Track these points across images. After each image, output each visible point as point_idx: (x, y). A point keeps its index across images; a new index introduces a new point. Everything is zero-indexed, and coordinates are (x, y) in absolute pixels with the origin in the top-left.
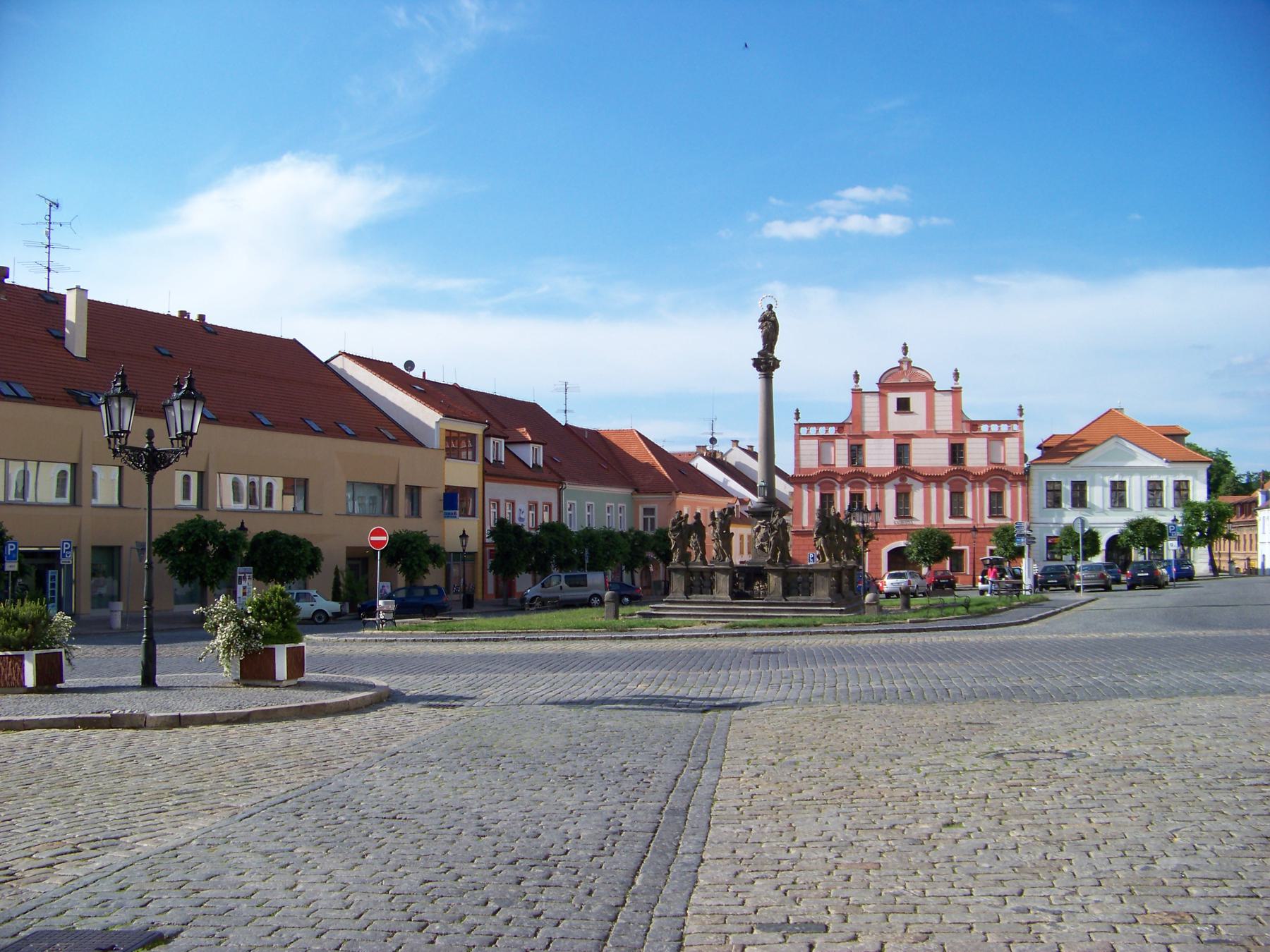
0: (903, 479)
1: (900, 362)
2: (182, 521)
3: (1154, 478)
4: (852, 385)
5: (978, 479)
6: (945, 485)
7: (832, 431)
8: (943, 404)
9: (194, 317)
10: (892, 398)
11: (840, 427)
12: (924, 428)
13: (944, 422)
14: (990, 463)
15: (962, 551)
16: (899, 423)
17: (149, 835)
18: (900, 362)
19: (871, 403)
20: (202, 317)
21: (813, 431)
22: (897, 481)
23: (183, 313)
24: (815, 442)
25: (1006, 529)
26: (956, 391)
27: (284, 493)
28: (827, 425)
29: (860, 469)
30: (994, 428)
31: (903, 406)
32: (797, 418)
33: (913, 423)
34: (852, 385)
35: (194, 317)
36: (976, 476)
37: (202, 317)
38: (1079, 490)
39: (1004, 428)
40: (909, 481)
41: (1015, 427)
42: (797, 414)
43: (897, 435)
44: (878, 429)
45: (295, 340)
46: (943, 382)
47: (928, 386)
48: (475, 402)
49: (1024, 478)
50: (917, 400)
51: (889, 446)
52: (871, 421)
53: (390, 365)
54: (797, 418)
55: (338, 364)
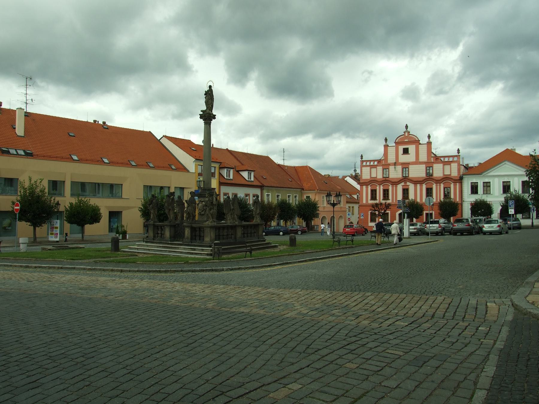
0: (405, 183)
1: (404, 132)
2: (101, 211)
3: (506, 180)
4: (384, 143)
5: (438, 181)
6: (381, 186)
7: (376, 163)
8: (423, 150)
9: (101, 122)
10: (401, 148)
11: (379, 161)
12: (414, 160)
13: (423, 157)
14: (371, 177)
15: (388, 213)
16: (403, 159)
17: (43, 333)
18: (404, 132)
19: (392, 151)
20: (104, 123)
21: (368, 164)
22: (403, 184)
23: (95, 121)
24: (369, 168)
25: (377, 204)
26: (429, 144)
27: (121, 197)
28: (374, 161)
29: (387, 179)
30: (446, 159)
31: (406, 151)
32: (362, 158)
33: (410, 158)
34: (427, 140)
35: (101, 122)
36: (436, 180)
37: (104, 123)
38: (487, 185)
39: (451, 159)
40: (408, 183)
41: (455, 159)
42: (362, 156)
43: (402, 164)
44: (414, 160)
45: (150, 132)
46: (424, 140)
47: (417, 142)
48: (235, 157)
49: (460, 180)
50: (412, 148)
51: (399, 168)
52: (391, 159)
53: (189, 142)
54: (362, 158)
55: (165, 142)
